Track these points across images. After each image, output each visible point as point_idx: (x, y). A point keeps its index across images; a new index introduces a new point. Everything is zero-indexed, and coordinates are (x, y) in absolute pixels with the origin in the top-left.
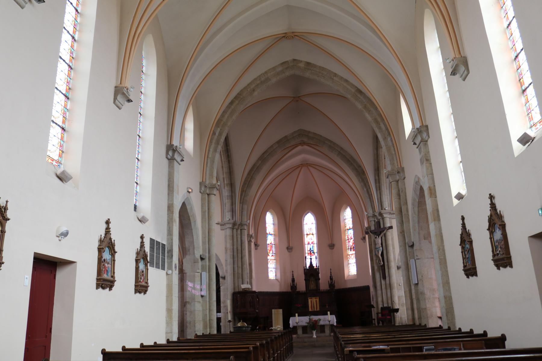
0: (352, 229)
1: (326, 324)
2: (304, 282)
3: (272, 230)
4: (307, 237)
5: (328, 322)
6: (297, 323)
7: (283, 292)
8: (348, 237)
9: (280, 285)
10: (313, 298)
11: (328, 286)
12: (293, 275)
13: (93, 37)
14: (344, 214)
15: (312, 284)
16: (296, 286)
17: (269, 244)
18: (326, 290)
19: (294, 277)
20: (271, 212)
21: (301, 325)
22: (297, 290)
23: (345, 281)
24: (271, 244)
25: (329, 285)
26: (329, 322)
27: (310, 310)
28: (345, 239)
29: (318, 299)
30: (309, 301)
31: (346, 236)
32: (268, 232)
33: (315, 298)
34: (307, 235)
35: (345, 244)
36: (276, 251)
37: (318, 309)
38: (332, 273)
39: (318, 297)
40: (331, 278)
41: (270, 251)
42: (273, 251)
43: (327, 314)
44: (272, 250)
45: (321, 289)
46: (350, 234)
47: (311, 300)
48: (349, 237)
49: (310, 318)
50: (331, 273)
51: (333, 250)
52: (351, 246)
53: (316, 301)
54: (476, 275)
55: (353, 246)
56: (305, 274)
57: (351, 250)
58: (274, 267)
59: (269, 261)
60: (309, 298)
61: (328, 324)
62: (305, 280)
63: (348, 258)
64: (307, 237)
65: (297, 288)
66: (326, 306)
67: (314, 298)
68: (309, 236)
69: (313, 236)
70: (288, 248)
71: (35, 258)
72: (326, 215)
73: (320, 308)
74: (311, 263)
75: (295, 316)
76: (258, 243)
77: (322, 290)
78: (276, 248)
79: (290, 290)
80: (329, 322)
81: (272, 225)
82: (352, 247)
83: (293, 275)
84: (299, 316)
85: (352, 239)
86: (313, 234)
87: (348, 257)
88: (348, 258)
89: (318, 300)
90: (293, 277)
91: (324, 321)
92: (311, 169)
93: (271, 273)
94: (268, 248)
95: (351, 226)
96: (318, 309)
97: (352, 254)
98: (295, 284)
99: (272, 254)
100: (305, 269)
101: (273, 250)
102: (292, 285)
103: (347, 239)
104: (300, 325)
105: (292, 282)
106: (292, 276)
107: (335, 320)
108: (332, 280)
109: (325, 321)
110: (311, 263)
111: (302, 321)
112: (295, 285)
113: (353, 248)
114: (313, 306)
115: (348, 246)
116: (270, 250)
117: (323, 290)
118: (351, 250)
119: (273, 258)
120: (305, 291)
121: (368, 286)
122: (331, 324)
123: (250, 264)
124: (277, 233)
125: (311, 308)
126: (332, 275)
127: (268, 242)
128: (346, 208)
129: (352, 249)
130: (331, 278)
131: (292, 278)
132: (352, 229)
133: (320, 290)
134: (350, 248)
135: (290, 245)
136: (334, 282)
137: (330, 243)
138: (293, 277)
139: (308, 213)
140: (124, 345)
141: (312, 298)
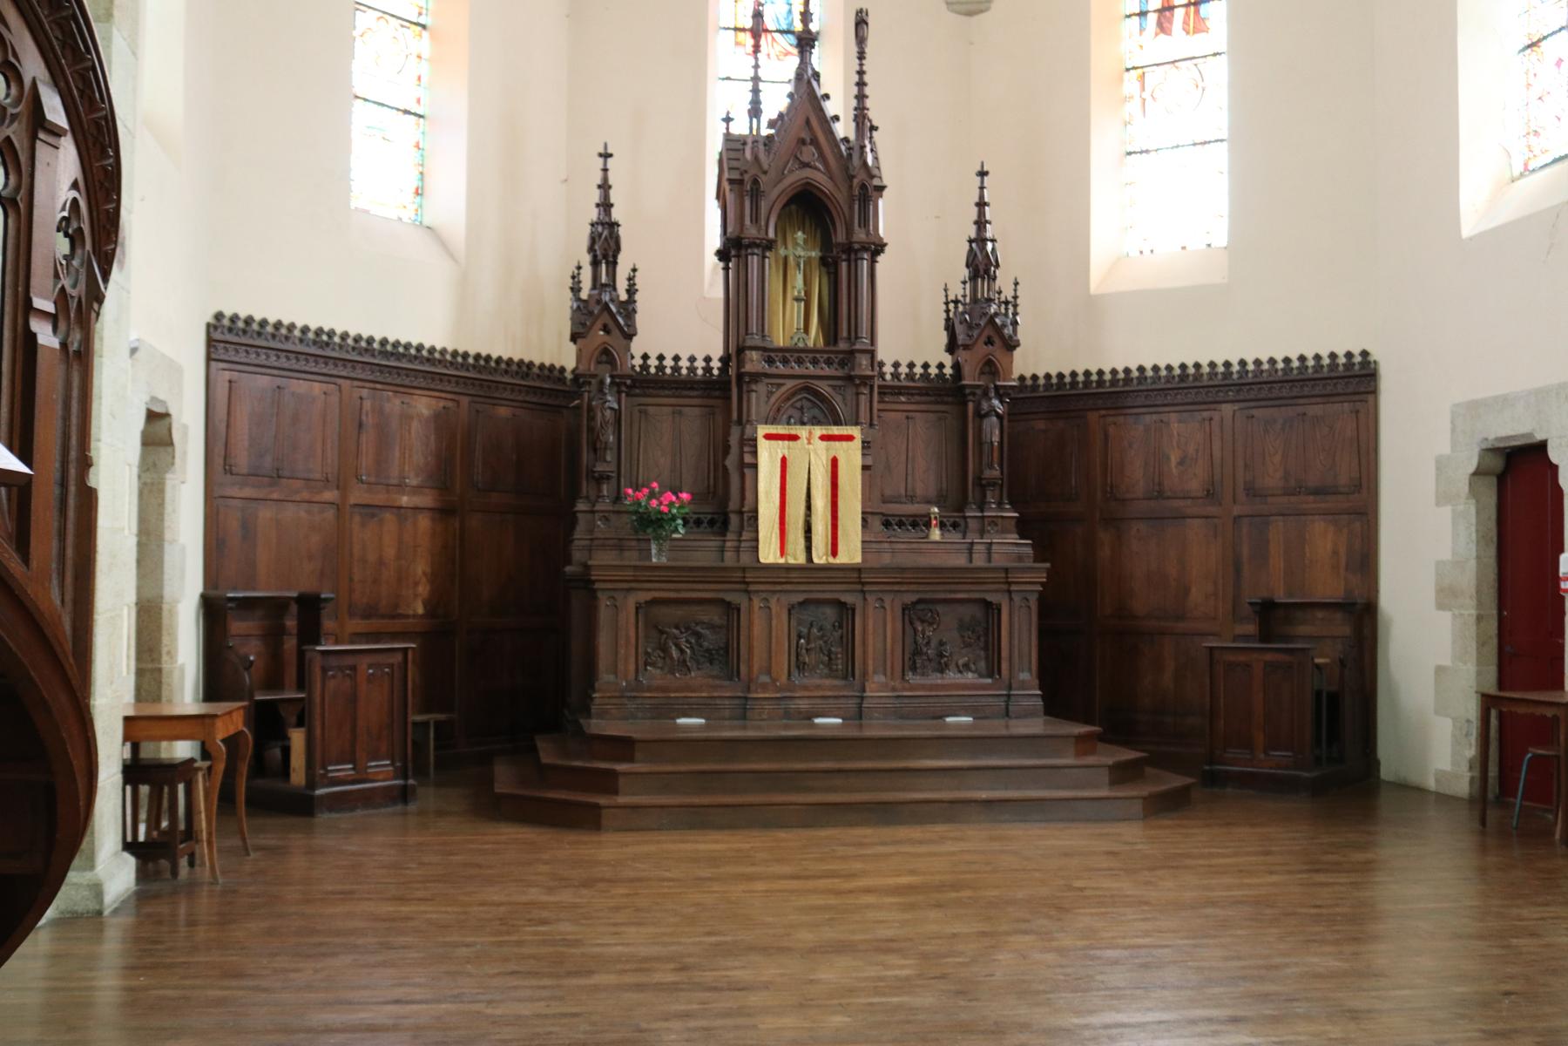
7: (483, 363)
10: (803, 431)
13: (353, 76)
16: (631, 300)
19: (616, 214)
22: (637, 347)
23: (1091, 308)
27: (769, 553)
30: (768, 455)
33: (824, 438)
37: (851, 553)
39: (855, 431)
40: (981, 265)
47: (781, 448)
57: (1163, 28)
60: (762, 430)
67: (818, 431)
71: (213, 343)
81: (569, 291)
89: (851, 456)
90: (605, 205)
98: (622, 285)
118: (1163, 28)
120: (716, 364)
123: (638, 460)
126: (990, 232)
130: (981, 265)
131: (594, 214)
138: (605, 205)
140: (1021, 342)
141: (794, 438)
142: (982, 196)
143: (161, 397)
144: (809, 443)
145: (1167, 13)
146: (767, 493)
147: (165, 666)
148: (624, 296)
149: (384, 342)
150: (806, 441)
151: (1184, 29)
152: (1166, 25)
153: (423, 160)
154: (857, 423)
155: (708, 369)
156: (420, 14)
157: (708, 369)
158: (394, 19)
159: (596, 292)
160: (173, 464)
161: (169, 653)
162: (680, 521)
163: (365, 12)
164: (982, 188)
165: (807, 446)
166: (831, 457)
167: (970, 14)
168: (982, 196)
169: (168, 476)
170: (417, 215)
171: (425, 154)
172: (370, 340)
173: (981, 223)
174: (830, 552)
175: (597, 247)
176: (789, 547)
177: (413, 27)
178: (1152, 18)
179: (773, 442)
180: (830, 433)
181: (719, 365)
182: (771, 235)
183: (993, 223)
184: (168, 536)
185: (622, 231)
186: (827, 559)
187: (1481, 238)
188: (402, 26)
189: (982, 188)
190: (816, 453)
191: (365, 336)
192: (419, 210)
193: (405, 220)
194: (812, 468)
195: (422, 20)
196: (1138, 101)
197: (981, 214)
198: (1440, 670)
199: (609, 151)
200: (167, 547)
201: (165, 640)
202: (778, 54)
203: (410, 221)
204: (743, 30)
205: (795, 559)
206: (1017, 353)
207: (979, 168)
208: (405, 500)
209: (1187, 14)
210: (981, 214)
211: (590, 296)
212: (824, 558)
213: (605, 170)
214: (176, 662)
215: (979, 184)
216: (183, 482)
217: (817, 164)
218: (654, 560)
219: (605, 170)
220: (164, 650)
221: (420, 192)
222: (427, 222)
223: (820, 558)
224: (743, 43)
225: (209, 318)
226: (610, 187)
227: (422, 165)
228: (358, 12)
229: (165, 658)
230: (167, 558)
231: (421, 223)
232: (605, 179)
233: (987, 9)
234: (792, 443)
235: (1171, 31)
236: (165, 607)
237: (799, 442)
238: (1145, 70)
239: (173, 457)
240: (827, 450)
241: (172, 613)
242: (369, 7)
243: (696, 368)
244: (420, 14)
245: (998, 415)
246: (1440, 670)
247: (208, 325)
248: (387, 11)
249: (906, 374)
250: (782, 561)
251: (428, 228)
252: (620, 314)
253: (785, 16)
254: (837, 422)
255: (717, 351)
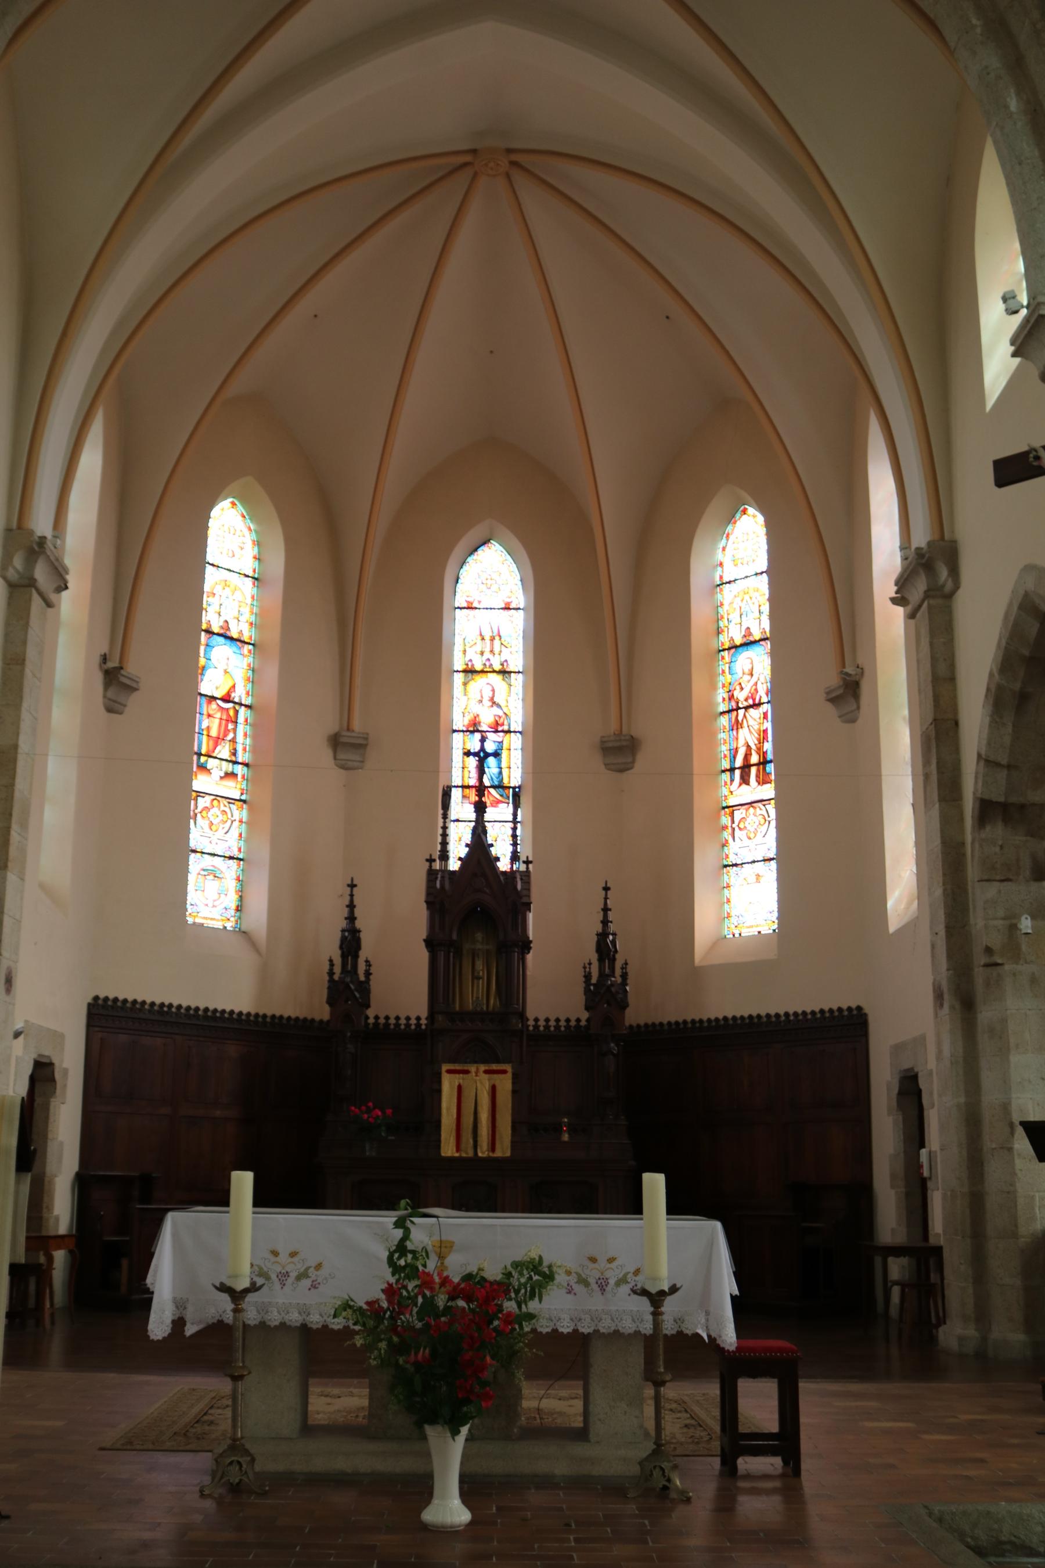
0: (768, 645)
1: (606, 1326)
2: (423, 956)
3: (247, 616)
4: (465, 684)
5: (644, 1305)
6: (237, 1296)
7: (277, 1021)
8: (731, 698)
9: (264, 975)
10: (473, 1068)
11: (580, 999)
12: (351, 906)
14: (712, 552)
15: (476, 978)
17: (213, 698)
18: (568, 1020)
19: (358, 924)
20: (245, 498)
21: (294, 1318)
22: (371, 1013)
23: (696, 975)
24: (226, 699)
25: (587, 991)
26: (656, 1314)
27: (448, 1149)
28: (712, 704)
29: (509, 1076)
30: (448, 1085)
31: (714, 688)
32: (211, 618)
33: (486, 1072)
34: (470, 671)
35: (713, 743)
36: (255, 750)
37: (503, 1150)
38: (611, 916)
39: (508, 1067)
40: (605, 949)
41: (217, 741)
42: (240, 748)
43: (634, 1205)
44: (233, 741)
45: (531, 1013)
46: (747, 677)
47: (457, 1079)
48: (741, 695)
49: (401, 1248)
50: (606, 910)
51: (625, 775)
52: (749, 747)
53: (493, 1089)
54: (226, 1203)
55: (759, 750)
56: (429, 903)
57: (745, 780)
58: (235, 853)
59: (206, 809)
60: (445, 1067)
61: (628, 1326)
62: (429, 943)
63: (725, 828)
64: (465, 684)
65: (373, 1003)
66: (557, 1129)
67: (483, 1067)
68: (479, 683)
69: (504, 685)
70: (336, 742)
72: (604, 578)
73: (514, 1144)
74: (479, 831)
75: (221, 1198)
76: (132, 668)
77: (536, 1020)
78: (257, 729)
79: (322, 1012)
80: (656, 1314)
82: (754, 759)
83: (351, 906)
84: (263, 1199)
85: (756, 705)
86: (504, 673)
87: (725, 820)
88: (725, 828)
89: (505, 1084)
90: (351, 918)
91: (583, 1281)
92: (532, 199)
93: (212, 886)
94: (205, 725)
95: (760, 624)
96: (503, 1150)
97: (751, 804)
99: (228, 767)
100: (432, 874)
101: (240, 738)
102: (336, 977)
103: (723, 707)
104: (274, 1318)
105: (344, 956)
106: (345, 912)
107: (728, 1285)
108: (613, 960)
109: (603, 1285)
110: (479, 831)
111: (303, 1276)
112: (362, 978)
113: (763, 763)
114: (468, 1121)
115: (724, 749)
116: (214, 733)
117: (547, 1020)
118: (745, 780)
119: (232, 789)
120: (423, 1022)
121: (859, 1008)
122: (669, 1328)
124: (274, 635)
125: (453, 1140)
126: (612, 928)
127: (211, 684)
128: (730, 518)
129: (754, 770)
130: (605, 949)
131: (344, 924)
132: (768, 645)
133: (522, 1016)
134: (739, 762)
135: (357, 725)
136: (624, 976)
137: (613, 727)
138: (351, 918)
139: (485, 543)
141: (467, 1072)
142: (606, 903)
143: (47, 1054)
144: (477, 1076)
145: (747, 770)
146: (448, 1109)
147: (45, 1215)
148: (362, 978)
149: (206, 1010)
150: (474, 1074)
151: (757, 781)
152: (746, 778)
153: (242, 888)
154: (509, 1062)
155: (418, 1025)
156: (242, 794)
157: (418, 1025)
158: (223, 799)
159: (343, 975)
160: (55, 1092)
161: (47, 1207)
162: (383, 1128)
163: (204, 797)
164: (606, 898)
165: (475, 1078)
166: (491, 1085)
167: (621, 771)
168: (606, 903)
169: (52, 1100)
170: (237, 924)
171: (243, 884)
172: (197, 1009)
173: (605, 922)
174: (490, 1149)
175: (344, 946)
176: (463, 1146)
177: (237, 803)
178: (737, 773)
179: (452, 1075)
180: (491, 1068)
181: (425, 1022)
182: (455, 937)
183: (613, 922)
184: (50, 1136)
185: (362, 935)
186: (488, 1154)
187: (899, 931)
188: (229, 803)
189: (606, 898)
190: (481, 1083)
191: (193, 1006)
192: (239, 921)
193: (228, 928)
194: (478, 1092)
195: (244, 797)
196: (730, 830)
197: (605, 916)
198: (893, 1230)
199: (355, 883)
200: (49, 1143)
201: (46, 1199)
202: (492, 802)
203: (231, 929)
204: (468, 787)
205: (467, 1153)
206: (628, 1011)
207: (604, 885)
208: (218, 1113)
209: (758, 770)
210: (605, 916)
211: (340, 978)
212: (486, 1153)
213: (352, 895)
214: (52, 1213)
215: (604, 896)
216: (63, 1103)
217: (485, 889)
218: (368, 1154)
219: (352, 895)
220: (45, 1205)
221: (239, 909)
222: (243, 929)
223: (483, 1153)
224: (468, 796)
225: (89, 1000)
226: (355, 906)
227: (241, 891)
228: (198, 798)
229: (45, 1210)
230: (49, 1149)
231: (240, 929)
232: (352, 901)
233: (631, 768)
234: (465, 1076)
235: (749, 782)
236: (47, 1179)
237: (469, 1075)
238: (734, 808)
239: (55, 1089)
240: (489, 1080)
241: (51, 1183)
242: (207, 794)
243: (400, 1025)
244: (242, 794)
245: (614, 1055)
246: (893, 1230)
247: (89, 1005)
248: (218, 794)
249: (554, 1027)
250: (457, 1155)
251: (244, 932)
252: (357, 991)
253: (497, 776)
254: (498, 1062)
255: (424, 1013)
